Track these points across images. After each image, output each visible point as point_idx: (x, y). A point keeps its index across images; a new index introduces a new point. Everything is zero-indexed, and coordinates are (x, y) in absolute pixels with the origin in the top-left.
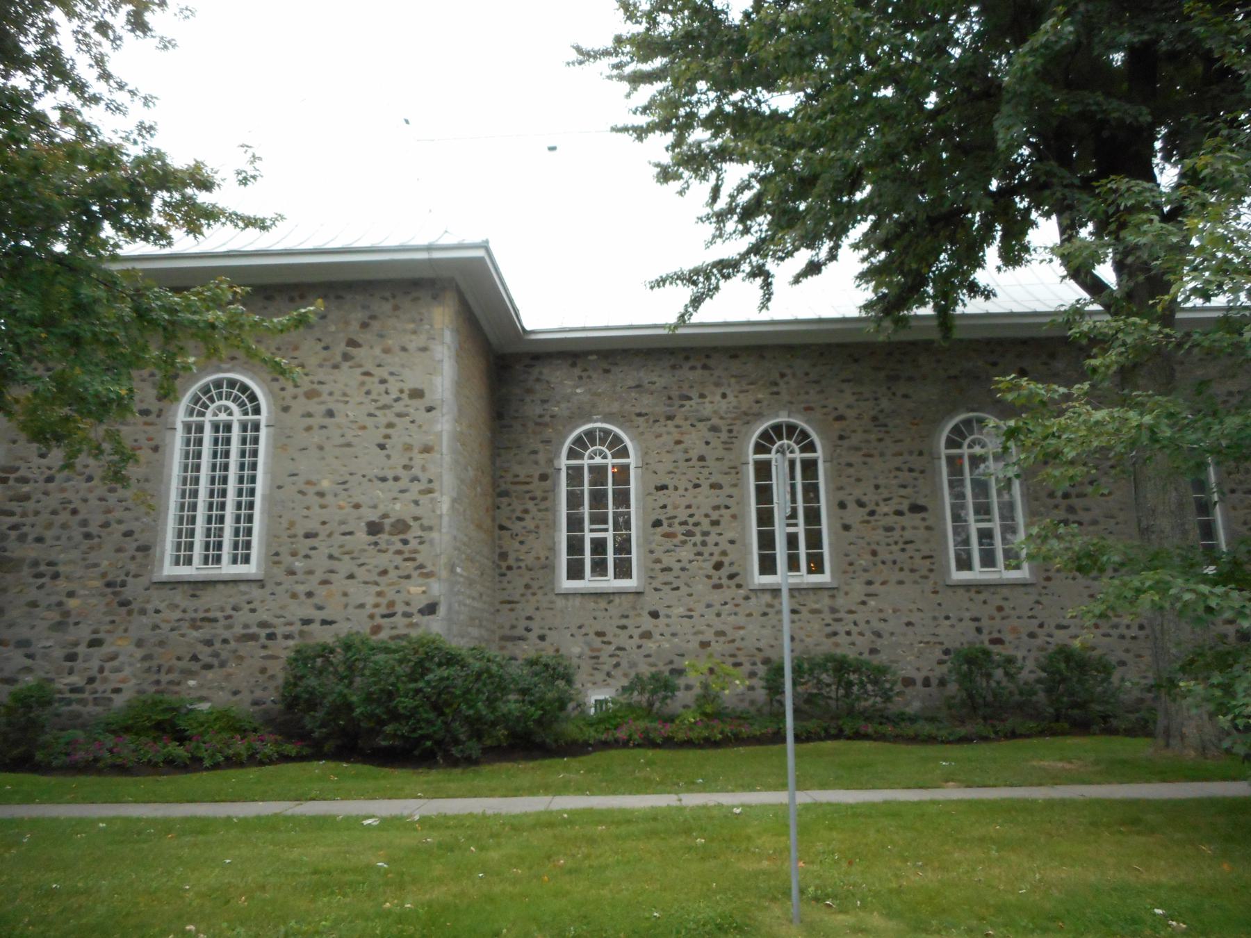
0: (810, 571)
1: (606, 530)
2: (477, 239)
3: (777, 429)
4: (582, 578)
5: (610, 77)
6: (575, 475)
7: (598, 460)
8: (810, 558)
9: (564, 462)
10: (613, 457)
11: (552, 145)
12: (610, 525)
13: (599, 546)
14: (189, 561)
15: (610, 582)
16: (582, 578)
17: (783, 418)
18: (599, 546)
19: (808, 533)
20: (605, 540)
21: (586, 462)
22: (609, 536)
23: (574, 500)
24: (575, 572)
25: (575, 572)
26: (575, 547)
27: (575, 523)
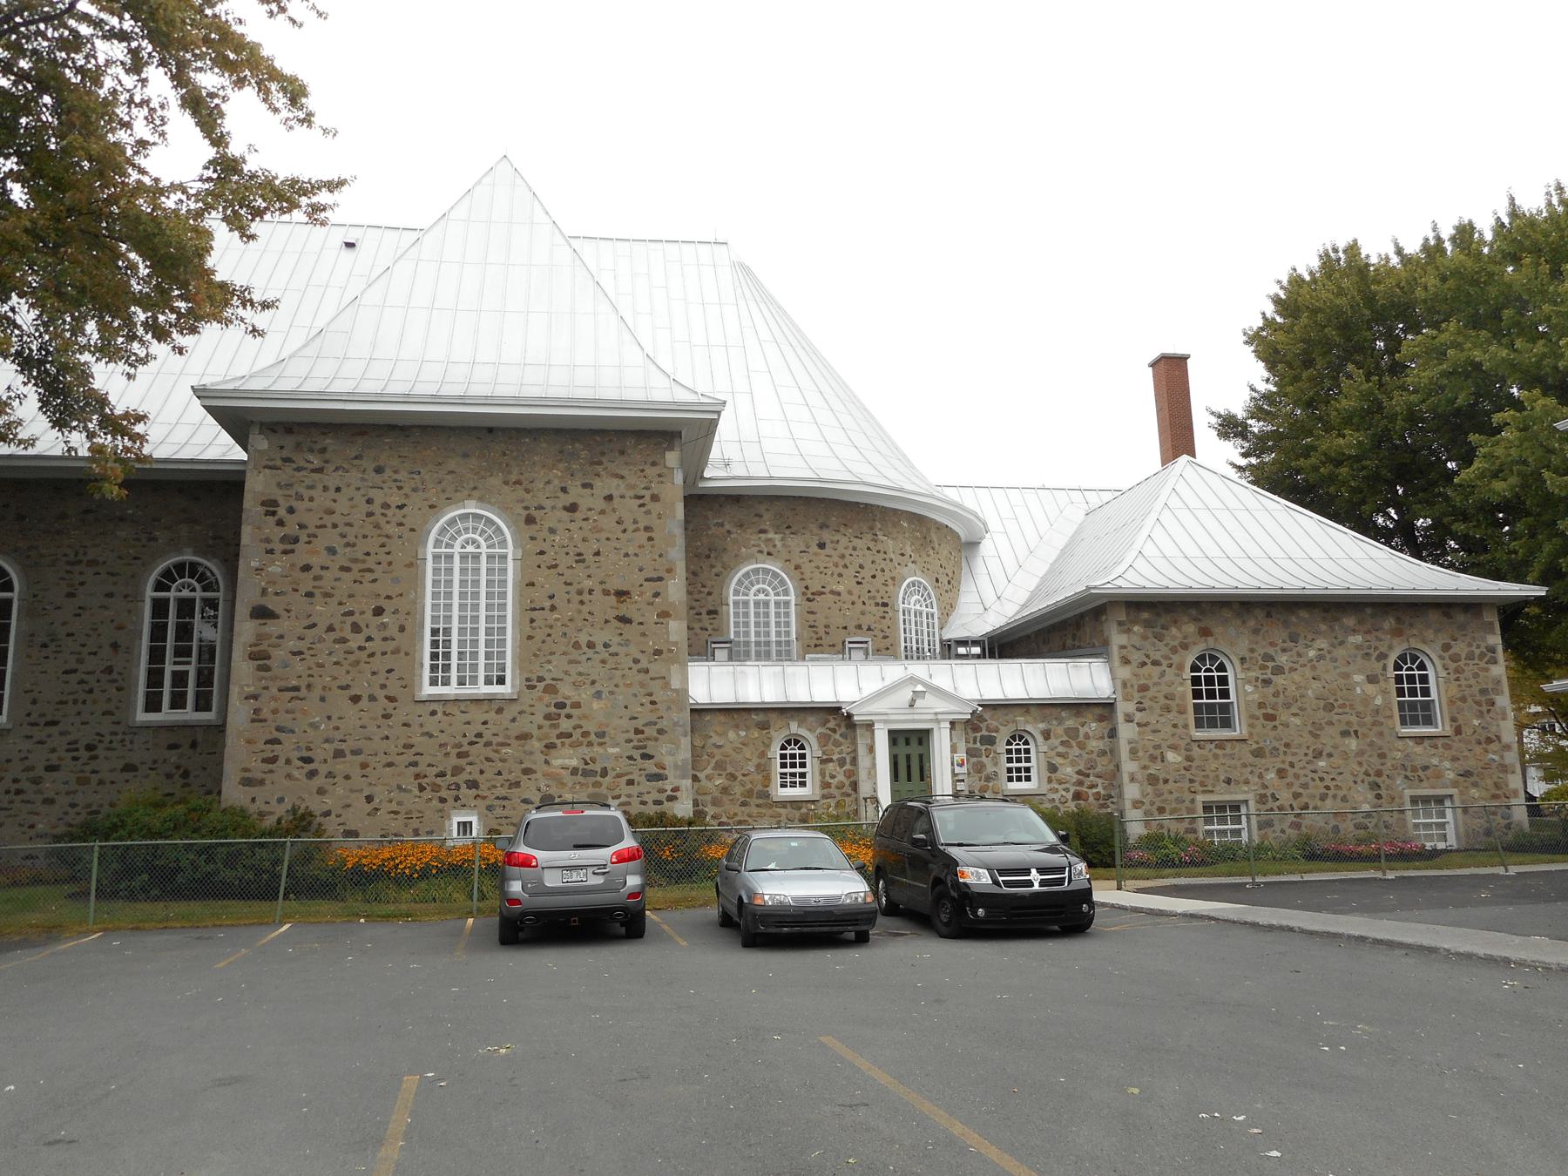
0: (197, 709)
1: (189, 663)
2: (1147, 378)
3: (180, 567)
4: (160, 710)
5: (333, 186)
6: (160, 608)
7: (186, 593)
8: (198, 695)
9: (150, 593)
10: (204, 590)
11: (350, 251)
12: (194, 659)
13: (180, 679)
14: (446, 682)
15: (189, 714)
16: (160, 710)
17: (188, 557)
18: (180, 679)
19: (199, 672)
20: (187, 672)
21: (172, 595)
22: (192, 670)
23: (158, 632)
24: (153, 704)
25: (153, 704)
26: (155, 678)
27: (157, 655)
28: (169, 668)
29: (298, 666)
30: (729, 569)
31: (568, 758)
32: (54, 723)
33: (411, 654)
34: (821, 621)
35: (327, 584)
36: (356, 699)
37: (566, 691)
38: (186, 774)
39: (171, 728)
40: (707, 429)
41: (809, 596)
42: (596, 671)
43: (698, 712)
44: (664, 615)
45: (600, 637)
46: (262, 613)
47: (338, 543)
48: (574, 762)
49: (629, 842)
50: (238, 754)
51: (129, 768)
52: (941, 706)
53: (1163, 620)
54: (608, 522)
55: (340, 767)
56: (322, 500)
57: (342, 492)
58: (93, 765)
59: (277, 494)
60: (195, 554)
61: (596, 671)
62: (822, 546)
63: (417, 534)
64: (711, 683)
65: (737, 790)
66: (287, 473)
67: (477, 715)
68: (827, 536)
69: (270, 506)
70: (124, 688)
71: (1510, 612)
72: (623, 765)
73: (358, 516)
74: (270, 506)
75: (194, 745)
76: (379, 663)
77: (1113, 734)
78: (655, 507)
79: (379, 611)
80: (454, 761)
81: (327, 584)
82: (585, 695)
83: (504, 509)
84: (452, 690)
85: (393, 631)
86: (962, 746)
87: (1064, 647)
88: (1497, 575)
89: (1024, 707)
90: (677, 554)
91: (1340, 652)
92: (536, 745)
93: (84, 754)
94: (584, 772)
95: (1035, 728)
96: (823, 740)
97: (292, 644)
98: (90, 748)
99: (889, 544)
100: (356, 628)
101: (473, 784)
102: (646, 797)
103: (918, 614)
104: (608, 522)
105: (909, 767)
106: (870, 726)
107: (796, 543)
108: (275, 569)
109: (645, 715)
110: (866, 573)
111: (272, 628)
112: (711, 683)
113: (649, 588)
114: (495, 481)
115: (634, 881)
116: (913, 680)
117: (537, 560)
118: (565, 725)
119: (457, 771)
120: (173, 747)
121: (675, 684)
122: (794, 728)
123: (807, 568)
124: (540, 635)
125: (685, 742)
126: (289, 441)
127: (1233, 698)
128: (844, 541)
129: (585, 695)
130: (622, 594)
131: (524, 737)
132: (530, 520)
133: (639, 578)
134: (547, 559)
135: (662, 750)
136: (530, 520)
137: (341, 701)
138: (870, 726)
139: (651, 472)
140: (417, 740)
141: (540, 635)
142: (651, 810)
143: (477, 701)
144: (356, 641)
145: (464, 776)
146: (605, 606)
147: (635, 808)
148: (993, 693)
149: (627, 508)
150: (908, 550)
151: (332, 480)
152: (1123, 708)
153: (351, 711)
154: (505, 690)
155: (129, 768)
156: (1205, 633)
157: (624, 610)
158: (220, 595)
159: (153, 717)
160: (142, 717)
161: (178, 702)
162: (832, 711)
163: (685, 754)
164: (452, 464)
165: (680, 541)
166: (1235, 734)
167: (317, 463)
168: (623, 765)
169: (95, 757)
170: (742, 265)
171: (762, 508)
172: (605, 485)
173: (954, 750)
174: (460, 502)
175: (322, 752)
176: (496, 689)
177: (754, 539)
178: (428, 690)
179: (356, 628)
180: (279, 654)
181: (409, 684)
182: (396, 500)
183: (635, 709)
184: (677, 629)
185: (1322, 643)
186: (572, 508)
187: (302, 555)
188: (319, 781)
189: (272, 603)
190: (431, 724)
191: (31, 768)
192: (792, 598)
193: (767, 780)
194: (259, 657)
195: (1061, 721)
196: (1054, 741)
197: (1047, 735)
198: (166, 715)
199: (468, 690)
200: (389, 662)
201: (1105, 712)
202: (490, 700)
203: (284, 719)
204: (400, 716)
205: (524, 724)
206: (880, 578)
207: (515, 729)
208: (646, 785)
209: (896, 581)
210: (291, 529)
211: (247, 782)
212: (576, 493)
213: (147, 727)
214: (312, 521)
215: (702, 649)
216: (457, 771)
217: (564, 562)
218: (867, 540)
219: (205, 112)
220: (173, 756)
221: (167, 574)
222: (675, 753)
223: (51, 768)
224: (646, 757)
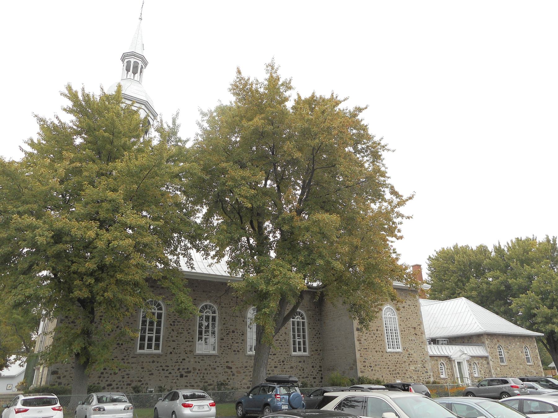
3: (206, 306)
7: (298, 320)
18: (150, 339)
24: (142, 347)
28: (147, 335)
31: (412, 368)
32: (274, 354)
36: (377, 351)
38: (303, 370)
39: (299, 357)
48: (413, 368)
50: (359, 365)
51: (292, 368)
53: (492, 338)
58: (285, 366)
60: (210, 302)
67: (397, 356)
71: (538, 339)
75: (304, 362)
77: (488, 363)
79: (377, 330)
80: (395, 367)
85: (380, 335)
87: (463, 343)
88: (533, 330)
91: (517, 346)
92: (407, 364)
93: (282, 363)
98: (283, 362)
101: (398, 373)
103: (298, 322)
118: (411, 359)
120: (300, 362)
124: (404, 337)
127: (503, 356)
131: (405, 362)
141: (404, 337)
145: (397, 371)
152: (490, 358)
155: (292, 368)
156: (498, 341)
159: (142, 351)
160: (139, 351)
161: (150, 347)
166: (505, 364)
169: (284, 364)
180: (362, 340)
185: (514, 344)
188: (374, 372)
191: (271, 367)
194: (359, 340)
220: (300, 364)
221: (203, 308)
223: (275, 367)
224: (424, 367)
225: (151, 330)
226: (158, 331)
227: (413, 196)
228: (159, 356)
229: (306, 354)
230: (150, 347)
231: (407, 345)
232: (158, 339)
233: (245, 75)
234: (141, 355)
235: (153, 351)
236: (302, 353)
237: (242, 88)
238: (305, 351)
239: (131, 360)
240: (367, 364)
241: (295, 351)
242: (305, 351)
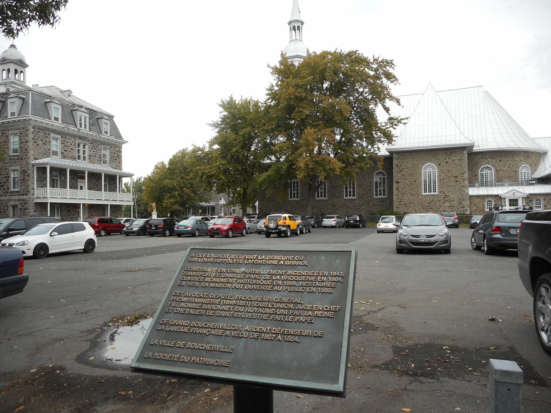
18: (350, 192)
24: (377, 195)
29: (403, 190)
30: (479, 167)
33: (421, 188)
34: (500, 176)
35: (407, 177)
37: (447, 193)
39: (380, 199)
40: (473, 147)
41: (497, 171)
42: (452, 190)
43: (470, 196)
44: (464, 180)
45: (452, 184)
46: (397, 182)
47: (408, 171)
49: (456, 216)
51: (374, 205)
52: (520, 195)
54: (453, 165)
55: (411, 205)
56: (405, 164)
57: (408, 163)
59: (398, 164)
61: (452, 190)
62: (500, 161)
63: (421, 168)
64: (473, 191)
65: (478, 209)
66: (399, 160)
67: (432, 197)
68: (501, 159)
69: (397, 165)
70: (372, 192)
72: (457, 205)
73: (411, 166)
74: (397, 165)
76: (416, 189)
78: (462, 161)
79: (415, 181)
81: (407, 177)
82: (450, 194)
83: (435, 163)
84: (428, 193)
86: (525, 202)
89: (540, 195)
90: (466, 169)
92: (442, 202)
94: (450, 206)
95: (542, 198)
96: (495, 201)
97: (402, 187)
99: (517, 159)
100: (412, 184)
101: (432, 208)
102: (461, 211)
104: (453, 165)
105: (240, 243)
106: (505, 198)
107: (494, 161)
108: (399, 175)
109: (461, 197)
110: (511, 165)
111: (399, 184)
112: (473, 191)
113: (461, 175)
114: (433, 159)
115: (457, 221)
116: (514, 190)
117: (441, 171)
118: (447, 199)
119: (429, 206)
121: (466, 192)
122: (489, 199)
123: (497, 166)
125: (468, 202)
126: (399, 155)
128: (506, 159)
129: (450, 194)
130: (456, 177)
131: (440, 201)
132: (439, 165)
133: (459, 174)
134: (443, 171)
135: (464, 203)
136: (439, 165)
137: (410, 196)
138: (505, 198)
139: (461, 155)
140: (423, 201)
142: (462, 213)
143: (432, 195)
144: (412, 186)
146: (453, 179)
147: (459, 212)
148: (532, 192)
149: (457, 162)
150: (523, 159)
151: (406, 160)
153: (412, 197)
154: (436, 193)
155: (374, 205)
157: (457, 179)
158: (385, 177)
160: (375, 197)
161: (321, 196)
162: (498, 196)
163: (468, 203)
164: (426, 156)
165: (467, 167)
167: (404, 158)
168: (457, 205)
170: (487, 92)
171: (486, 154)
172: (452, 158)
173: (523, 202)
174: (427, 163)
175: (408, 203)
176: (434, 193)
177: (485, 161)
178: (424, 194)
179: (412, 184)
180: (400, 188)
181: (421, 193)
182: (417, 163)
183: (459, 196)
184: (466, 182)
186: (447, 162)
187: (402, 173)
189: (399, 181)
190: (424, 199)
192: (493, 172)
193: (484, 208)
194: (397, 189)
195: (548, 197)
196: (546, 201)
197: (544, 200)
198: (379, 197)
199: (430, 193)
200: (417, 189)
201: (515, 203)
202: (434, 195)
203: (402, 198)
204: (419, 198)
205: (440, 199)
206: (515, 166)
207: (438, 200)
208: (461, 209)
209: (519, 166)
210: (401, 169)
211: (397, 208)
212: (447, 160)
213: (376, 198)
214: (404, 167)
215: (472, 185)
216: (429, 206)
217: (446, 172)
218: (511, 159)
219: (387, 110)
220: (380, 203)
222: (466, 203)
225: (294, 190)
226: (298, 190)
227: (400, 105)
228: (298, 201)
229: (385, 197)
230: (321, 196)
231: (445, 189)
232: (297, 193)
233: (272, 65)
234: (291, 201)
235: (296, 199)
236: (352, 197)
237: (276, 71)
238: (325, 196)
239: (287, 203)
240: (402, 203)
241: (377, 195)
242: (384, 195)
